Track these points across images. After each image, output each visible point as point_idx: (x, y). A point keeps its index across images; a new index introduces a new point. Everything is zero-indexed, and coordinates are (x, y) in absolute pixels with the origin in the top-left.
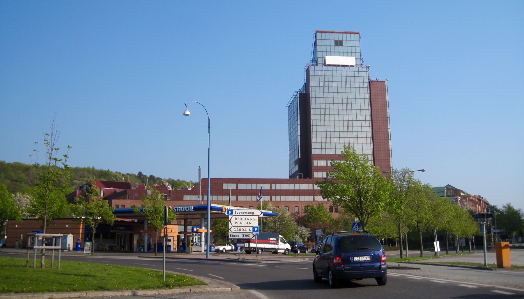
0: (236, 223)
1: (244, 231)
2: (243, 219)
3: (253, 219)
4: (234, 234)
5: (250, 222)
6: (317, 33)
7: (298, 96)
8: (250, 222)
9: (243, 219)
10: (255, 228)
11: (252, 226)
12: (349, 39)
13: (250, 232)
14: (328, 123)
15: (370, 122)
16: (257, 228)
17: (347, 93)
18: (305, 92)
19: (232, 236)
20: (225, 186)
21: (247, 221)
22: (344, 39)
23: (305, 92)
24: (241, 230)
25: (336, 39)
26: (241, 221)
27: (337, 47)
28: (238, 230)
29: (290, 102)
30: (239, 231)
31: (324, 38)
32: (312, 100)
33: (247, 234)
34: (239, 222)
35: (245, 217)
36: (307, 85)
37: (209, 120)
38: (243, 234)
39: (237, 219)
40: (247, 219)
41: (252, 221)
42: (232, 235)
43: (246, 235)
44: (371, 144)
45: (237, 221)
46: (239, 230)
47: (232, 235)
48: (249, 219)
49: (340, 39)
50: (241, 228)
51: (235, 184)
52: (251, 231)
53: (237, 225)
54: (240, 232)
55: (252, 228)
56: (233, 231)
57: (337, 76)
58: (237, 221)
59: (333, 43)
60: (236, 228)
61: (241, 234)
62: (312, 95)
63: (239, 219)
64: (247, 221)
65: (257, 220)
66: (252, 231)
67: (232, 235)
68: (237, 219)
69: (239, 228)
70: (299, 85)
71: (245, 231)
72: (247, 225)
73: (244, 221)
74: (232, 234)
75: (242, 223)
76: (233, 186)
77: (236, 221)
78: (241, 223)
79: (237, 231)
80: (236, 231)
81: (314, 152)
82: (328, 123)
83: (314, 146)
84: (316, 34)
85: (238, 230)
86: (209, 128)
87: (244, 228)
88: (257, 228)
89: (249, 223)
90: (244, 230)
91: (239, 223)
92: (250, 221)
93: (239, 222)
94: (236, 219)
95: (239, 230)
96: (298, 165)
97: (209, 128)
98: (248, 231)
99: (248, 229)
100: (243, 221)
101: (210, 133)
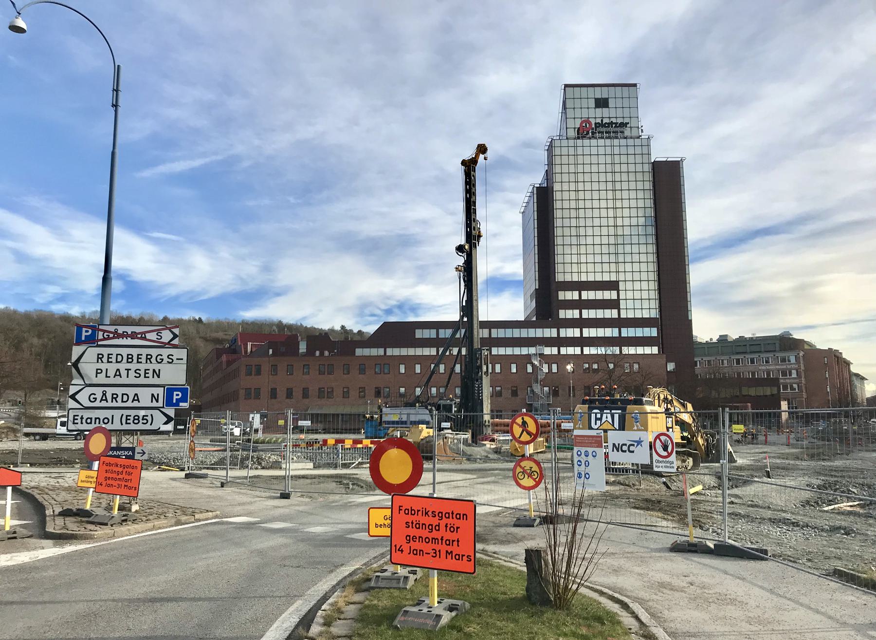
0: (98, 372)
1: (129, 404)
2: (130, 358)
3: (166, 360)
4: (87, 414)
5: (154, 371)
6: (566, 88)
7: (535, 192)
8: (154, 371)
9: (130, 358)
10: (175, 393)
11: (163, 386)
12: (619, 95)
13: (155, 404)
14: (582, 231)
15: (654, 245)
16: (184, 391)
17: (613, 172)
18: (546, 186)
19: (79, 421)
20: (419, 334)
21: (142, 367)
22: (612, 95)
23: (546, 186)
24: (119, 399)
25: (598, 96)
26: (118, 366)
27: (599, 110)
28: (104, 397)
29: (524, 205)
30: (109, 404)
31: (577, 95)
32: (557, 196)
33: (142, 413)
34: (112, 368)
35: (135, 352)
36: (549, 175)
37: (118, 69)
38: (126, 412)
39: (105, 359)
40: (143, 360)
41: (165, 368)
42: (82, 418)
43: (136, 419)
44: (657, 301)
45: (103, 366)
46: (109, 399)
47: (79, 418)
48: (153, 360)
49: (605, 96)
50: (119, 391)
51: (435, 331)
52: (157, 401)
53: (101, 379)
54: (114, 404)
55: (160, 391)
56: (87, 404)
57: (624, 262)
58: (103, 366)
59: (592, 103)
60: (98, 391)
61: (118, 414)
62: (557, 187)
63: (114, 360)
64: (142, 367)
65: (185, 361)
66: (160, 404)
67: (82, 418)
68: (105, 359)
69: (110, 391)
70: (538, 179)
71: (136, 404)
72: (142, 380)
73: (133, 366)
74: (80, 413)
75: (124, 373)
76: (431, 334)
77: (100, 366)
78: (118, 373)
79: (104, 404)
80: (97, 404)
81: (560, 278)
82: (582, 231)
83: (559, 268)
84: (565, 89)
85: (136, 398)
86: (116, 90)
87: (131, 391)
88: (184, 391)
89: (151, 372)
90: (99, 399)
91: (111, 373)
92: (157, 367)
93: (112, 368)
94: (100, 357)
95: (109, 399)
96: (534, 301)
97: (116, 90)
98: (145, 401)
99: (145, 395)
100: (129, 366)
101: (120, 109)
